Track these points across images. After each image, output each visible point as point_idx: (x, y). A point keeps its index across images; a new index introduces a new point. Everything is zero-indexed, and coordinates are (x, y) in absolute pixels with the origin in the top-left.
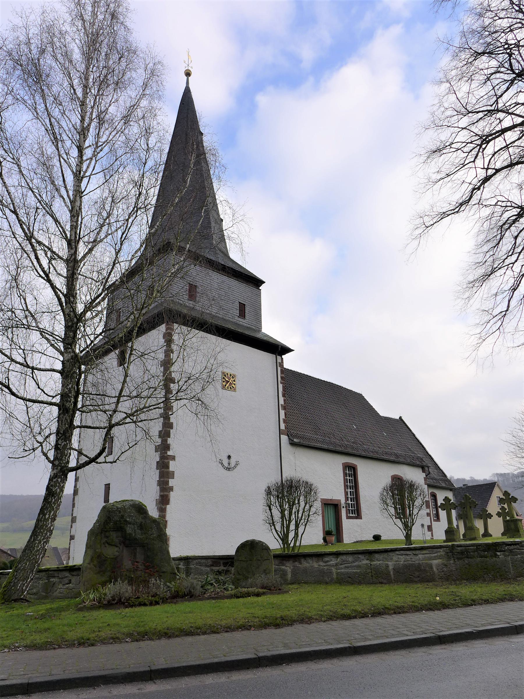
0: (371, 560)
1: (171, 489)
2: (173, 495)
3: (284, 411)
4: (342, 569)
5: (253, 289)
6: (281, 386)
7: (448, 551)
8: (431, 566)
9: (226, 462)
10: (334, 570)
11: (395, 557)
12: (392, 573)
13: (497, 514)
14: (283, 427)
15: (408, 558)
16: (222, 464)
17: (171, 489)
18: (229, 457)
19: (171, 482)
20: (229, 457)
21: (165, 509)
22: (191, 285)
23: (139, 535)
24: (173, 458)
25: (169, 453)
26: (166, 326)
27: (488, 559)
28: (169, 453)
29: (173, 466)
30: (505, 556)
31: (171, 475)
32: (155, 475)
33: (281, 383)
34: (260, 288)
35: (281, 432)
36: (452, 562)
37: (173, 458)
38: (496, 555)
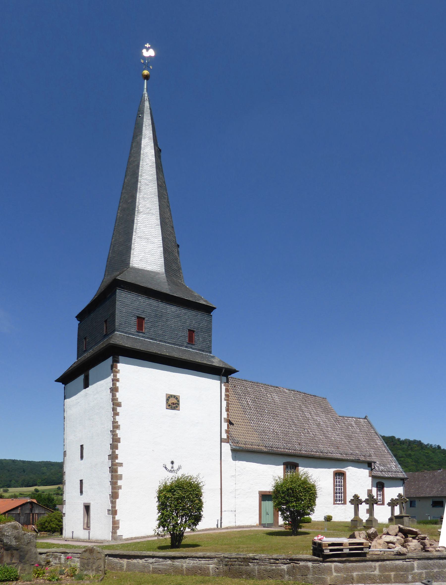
0: (173, 562)
1: (120, 487)
2: (121, 492)
3: (226, 424)
4: (156, 565)
5: (205, 317)
6: (224, 403)
7: (220, 560)
8: (208, 569)
9: (169, 466)
10: (151, 566)
11: (187, 561)
12: (185, 570)
13: (387, 504)
14: (224, 436)
15: (195, 562)
16: (166, 468)
17: (120, 487)
18: (172, 463)
19: (120, 483)
20: (172, 463)
21: (115, 502)
22: (138, 318)
23: (14, 543)
24: (121, 464)
25: (117, 461)
26: (113, 358)
27: (243, 567)
28: (117, 461)
29: (120, 471)
30: (254, 565)
31: (120, 477)
32: (108, 476)
33: (225, 400)
34: (212, 314)
35: (222, 441)
36: (221, 567)
37: (121, 464)
38: (248, 565)
